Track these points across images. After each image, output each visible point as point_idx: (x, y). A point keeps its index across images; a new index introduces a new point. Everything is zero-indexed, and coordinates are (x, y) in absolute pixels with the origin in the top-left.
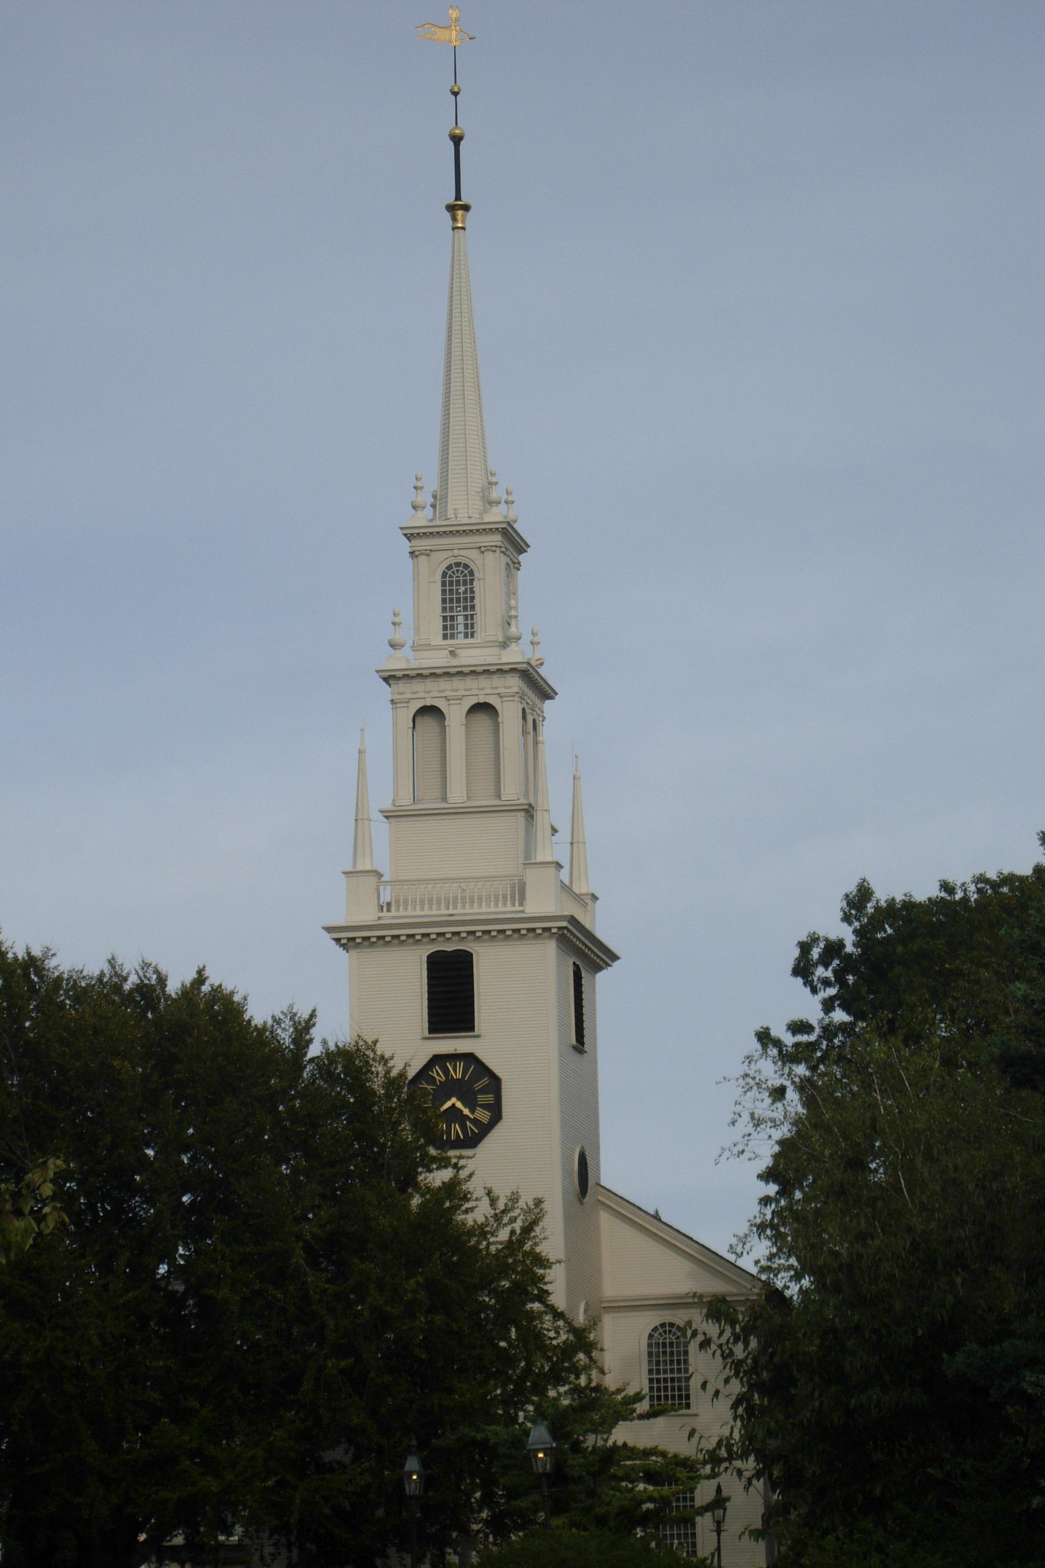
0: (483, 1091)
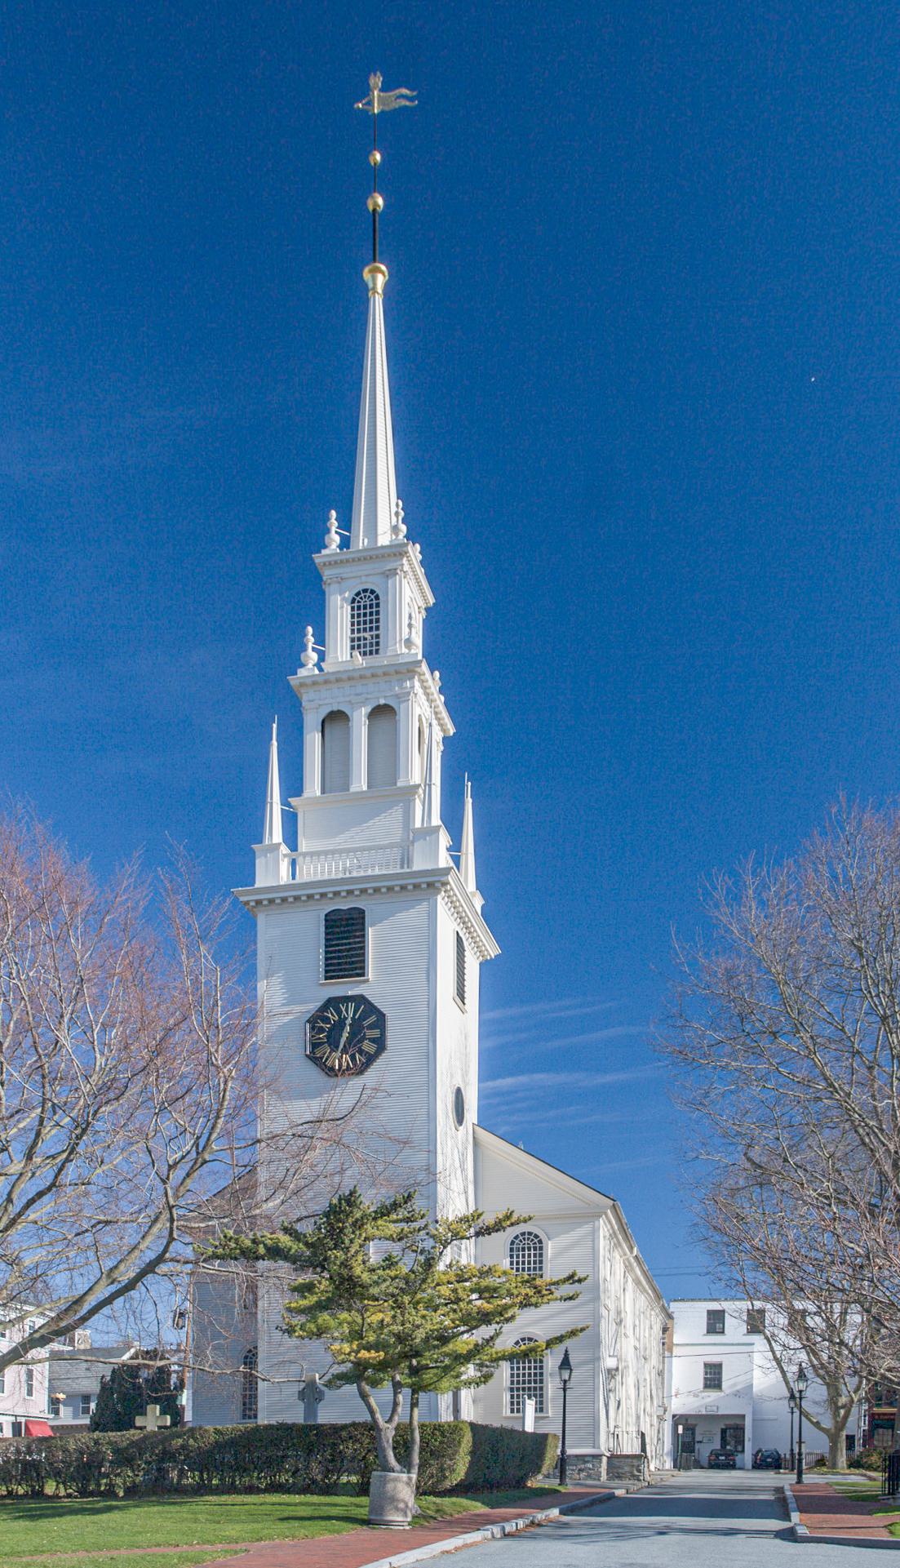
0: (370, 1027)
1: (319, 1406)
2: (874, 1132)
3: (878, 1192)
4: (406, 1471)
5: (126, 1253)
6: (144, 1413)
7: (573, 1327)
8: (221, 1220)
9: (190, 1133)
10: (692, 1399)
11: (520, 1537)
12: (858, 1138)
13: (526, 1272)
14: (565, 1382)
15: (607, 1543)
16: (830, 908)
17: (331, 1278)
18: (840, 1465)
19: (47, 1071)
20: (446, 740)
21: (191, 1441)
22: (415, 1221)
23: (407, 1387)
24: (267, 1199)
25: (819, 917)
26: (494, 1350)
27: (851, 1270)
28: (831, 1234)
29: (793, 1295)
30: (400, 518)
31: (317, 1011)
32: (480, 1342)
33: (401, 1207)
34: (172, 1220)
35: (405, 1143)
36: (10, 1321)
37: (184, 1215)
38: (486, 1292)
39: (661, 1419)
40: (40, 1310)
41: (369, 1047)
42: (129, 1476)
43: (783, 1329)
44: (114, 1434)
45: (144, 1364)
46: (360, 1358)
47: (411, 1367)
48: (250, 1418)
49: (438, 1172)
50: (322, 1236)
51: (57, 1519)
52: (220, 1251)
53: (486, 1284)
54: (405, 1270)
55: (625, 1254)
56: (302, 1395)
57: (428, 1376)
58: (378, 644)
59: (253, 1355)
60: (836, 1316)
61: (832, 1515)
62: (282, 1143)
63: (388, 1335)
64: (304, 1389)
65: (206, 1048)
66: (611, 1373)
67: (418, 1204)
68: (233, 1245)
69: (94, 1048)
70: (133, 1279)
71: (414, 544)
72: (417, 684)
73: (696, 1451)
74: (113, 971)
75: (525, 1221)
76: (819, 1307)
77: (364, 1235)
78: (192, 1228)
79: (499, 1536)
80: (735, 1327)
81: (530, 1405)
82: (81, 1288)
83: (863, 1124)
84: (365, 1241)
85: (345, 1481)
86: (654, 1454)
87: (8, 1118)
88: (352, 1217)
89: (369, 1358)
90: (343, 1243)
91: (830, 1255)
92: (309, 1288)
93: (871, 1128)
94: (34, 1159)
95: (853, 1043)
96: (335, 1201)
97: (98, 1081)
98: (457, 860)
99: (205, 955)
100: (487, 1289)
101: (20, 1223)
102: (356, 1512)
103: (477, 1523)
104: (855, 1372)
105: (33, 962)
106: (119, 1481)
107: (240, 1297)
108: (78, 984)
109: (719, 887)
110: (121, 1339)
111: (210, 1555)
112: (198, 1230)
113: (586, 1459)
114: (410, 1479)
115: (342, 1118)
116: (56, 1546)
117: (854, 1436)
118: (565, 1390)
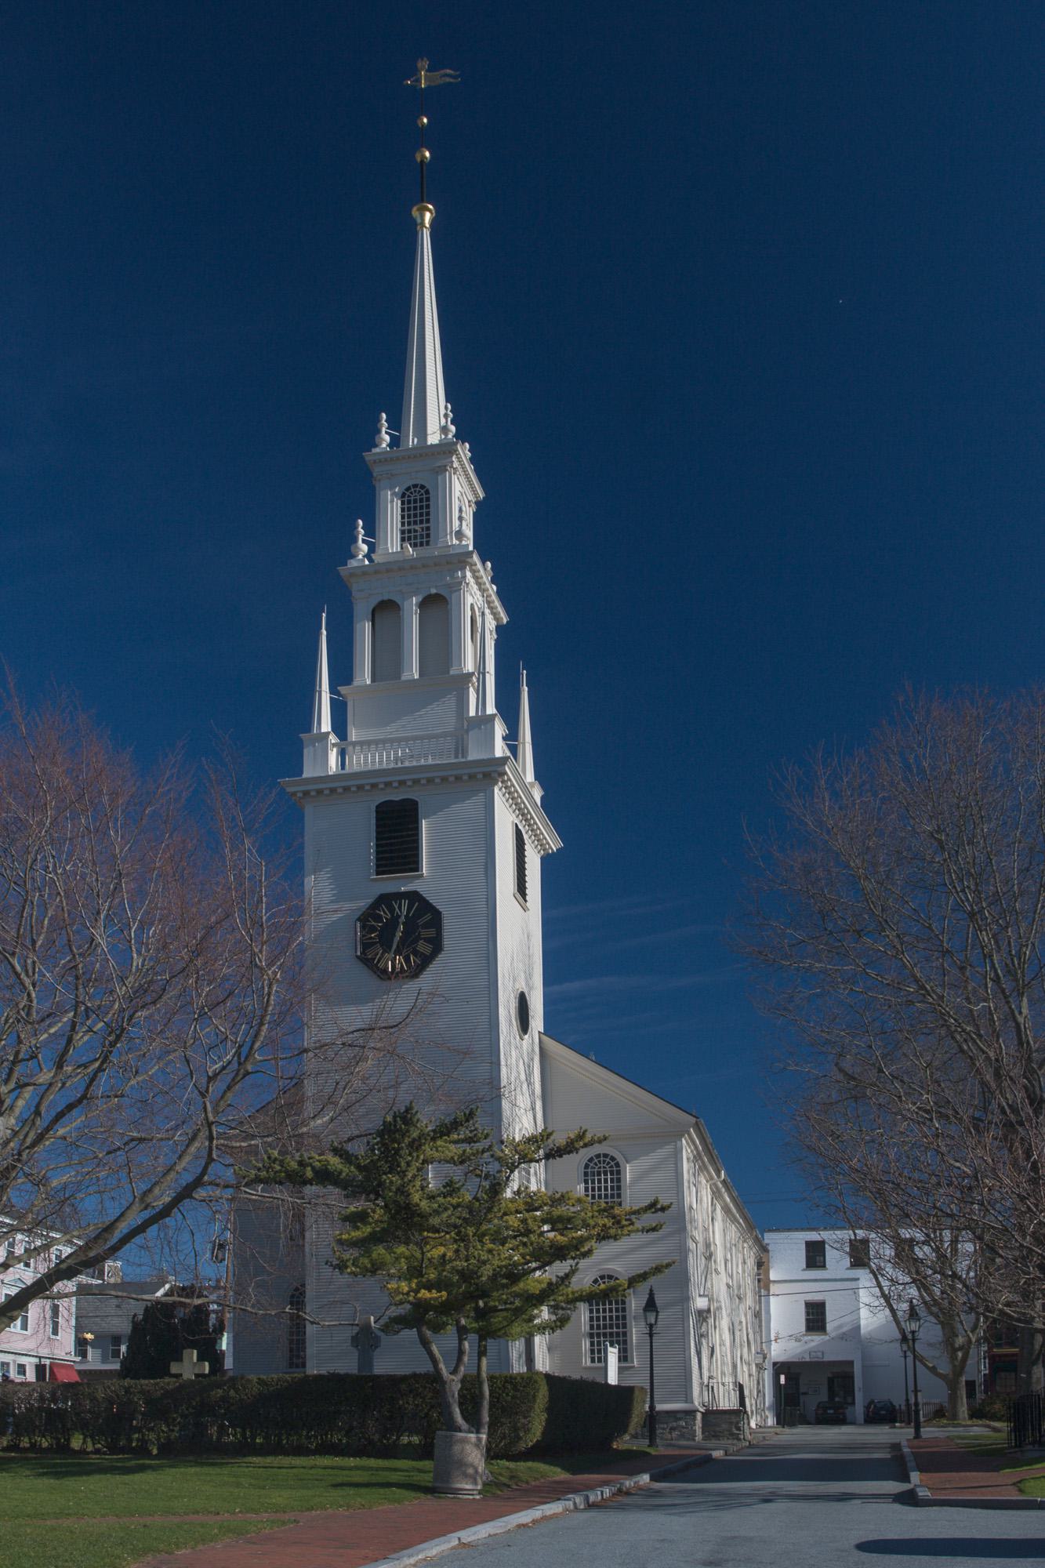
0: (426, 926)
1: (375, 1353)
2: (972, 1038)
3: (982, 1105)
4: (474, 1431)
5: (160, 1175)
6: (179, 1359)
7: (658, 1262)
8: (265, 1139)
9: (231, 1041)
10: (793, 1344)
11: (606, 1507)
12: (955, 1044)
13: (603, 1200)
14: (651, 1326)
15: (705, 1514)
16: (906, 799)
17: (386, 1206)
18: (961, 1415)
19: (81, 971)
20: (499, 628)
21: (232, 1393)
22: (478, 1141)
23: (474, 1333)
24: (315, 1116)
25: (895, 809)
26: (570, 1289)
27: (959, 1192)
28: (935, 1153)
29: (898, 1222)
30: (449, 419)
31: (368, 909)
32: (554, 1280)
33: (462, 1125)
34: (211, 1138)
35: (465, 1054)
36: (35, 1249)
37: (225, 1133)
38: (559, 1223)
39: (760, 1367)
40: (68, 1237)
41: (424, 947)
42: (163, 1431)
43: (889, 1261)
44: (147, 1382)
45: (181, 1302)
46: (420, 1299)
47: (477, 1309)
48: (297, 1367)
49: (502, 1085)
50: (376, 1158)
51: (85, 1478)
52: (263, 1174)
53: (559, 1213)
54: (468, 1197)
55: (712, 1178)
56: (355, 1340)
57: (496, 1320)
58: (428, 536)
59: (301, 1294)
60: (946, 1245)
61: (954, 1474)
62: (330, 1054)
63: (451, 1273)
64: (358, 1334)
65: (249, 948)
66: (703, 1315)
67: (480, 1122)
68: (278, 1168)
69: (131, 948)
70: (168, 1204)
71: (463, 443)
72: (468, 574)
73: (801, 1404)
74: (153, 865)
75: (600, 1142)
76: (927, 1235)
77: (422, 1157)
78: (233, 1147)
79: (582, 1507)
80: (837, 1260)
81: (613, 1355)
82: (113, 1212)
83: (959, 1030)
84: (423, 1164)
85: (406, 1442)
86: (754, 1408)
87: (38, 1023)
88: (409, 1137)
89: (430, 1299)
90: (399, 1166)
91: (936, 1176)
92: (359, 1218)
93: (968, 1033)
94: (65, 1069)
95: (942, 941)
96: (389, 1119)
97: (135, 982)
98: (514, 750)
99: (249, 849)
100: (560, 1219)
101: (48, 1139)
102: (418, 1478)
103: (555, 1492)
104: (971, 1309)
105: (70, 855)
106: (152, 1436)
107: (286, 1227)
108: (116, 878)
109: (789, 778)
110: (155, 1273)
111: (255, 1526)
112: (239, 1150)
113: (679, 1416)
114: (479, 1440)
115: (397, 1026)
116: (83, 1509)
117: (974, 1381)
118: (651, 1335)
